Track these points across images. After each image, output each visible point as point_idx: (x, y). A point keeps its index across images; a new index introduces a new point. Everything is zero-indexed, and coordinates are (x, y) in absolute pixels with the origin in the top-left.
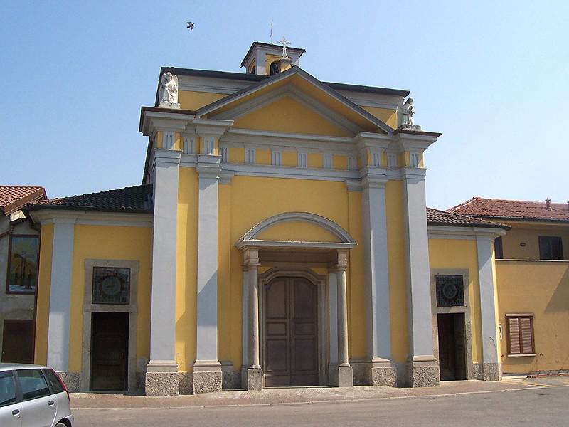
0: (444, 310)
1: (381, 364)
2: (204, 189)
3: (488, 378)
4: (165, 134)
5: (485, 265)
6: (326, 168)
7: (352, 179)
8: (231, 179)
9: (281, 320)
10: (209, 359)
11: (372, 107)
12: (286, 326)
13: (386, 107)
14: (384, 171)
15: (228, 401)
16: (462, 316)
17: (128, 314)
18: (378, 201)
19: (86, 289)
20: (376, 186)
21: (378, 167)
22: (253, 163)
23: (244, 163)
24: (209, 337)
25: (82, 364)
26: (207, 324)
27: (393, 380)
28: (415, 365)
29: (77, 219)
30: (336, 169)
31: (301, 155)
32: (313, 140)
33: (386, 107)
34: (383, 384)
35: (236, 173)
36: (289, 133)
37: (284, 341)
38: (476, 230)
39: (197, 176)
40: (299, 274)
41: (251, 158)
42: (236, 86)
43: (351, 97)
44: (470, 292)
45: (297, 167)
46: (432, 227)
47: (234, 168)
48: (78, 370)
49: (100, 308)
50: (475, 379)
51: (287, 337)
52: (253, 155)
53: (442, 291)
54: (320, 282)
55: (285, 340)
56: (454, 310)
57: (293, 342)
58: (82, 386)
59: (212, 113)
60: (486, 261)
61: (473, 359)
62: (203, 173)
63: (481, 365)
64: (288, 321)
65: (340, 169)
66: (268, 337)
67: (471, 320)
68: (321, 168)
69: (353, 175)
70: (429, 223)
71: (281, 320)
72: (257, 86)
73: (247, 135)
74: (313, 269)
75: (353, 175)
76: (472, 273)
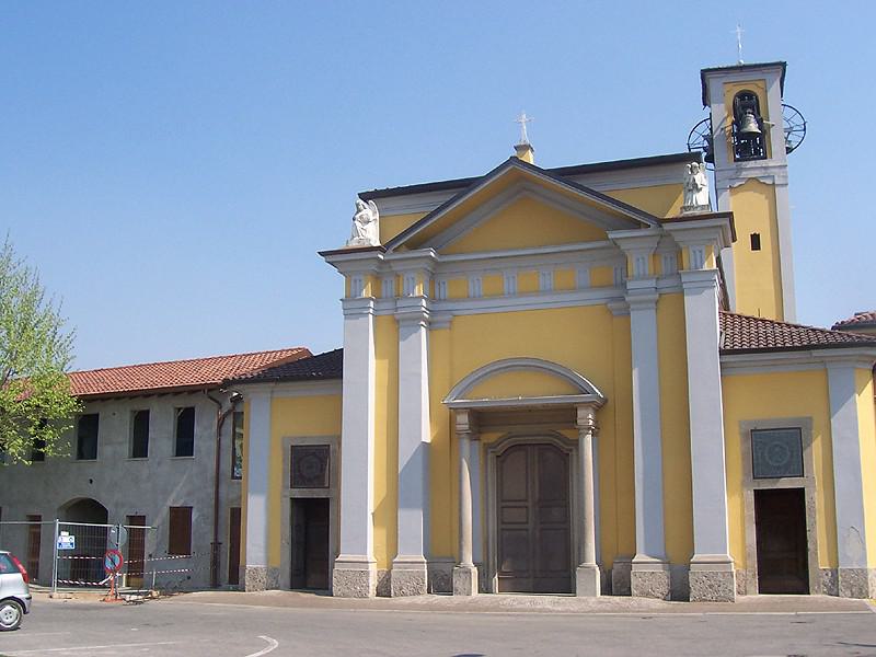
0: (766, 485)
1: (646, 566)
2: (406, 338)
3: (847, 593)
4: (353, 278)
5: (844, 407)
6: (514, 293)
7: (613, 299)
8: (451, 322)
9: (508, 504)
10: (413, 554)
11: (636, 194)
12: (527, 512)
13: (668, 182)
14: (653, 283)
15: (431, 608)
16: (800, 493)
17: (328, 499)
18: (644, 325)
19: (284, 472)
20: (643, 306)
21: (644, 277)
22: (644, 274)
23: (468, 298)
24: (413, 522)
25: (283, 559)
26: (409, 506)
27: (665, 589)
28: (635, 568)
29: (272, 392)
30: (592, 288)
31: (508, 278)
32: (579, 250)
33: (668, 182)
34: (647, 595)
35: (456, 313)
36: (524, 248)
37: (525, 532)
38: (814, 354)
39: (396, 326)
40: (547, 440)
41: (511, 287)
42: (439, 199)
43: (587, 181)
44: (815, 454)
45: (538, 293)
46: (728, 358)
47: (450, 306)
48: (276, 564)
49: (299, 493)
50: (824, 593)
51: (530, 526)
52: (644, 264)
53: (762, 454)
54: (571, 450)
55: (527, 530)
56: (785, 483)
57: (538, 534)
58: (281, 581)
59: (411, 241)
60: (847, 399)
61: (819, 560)
62: (404, 320)
63: (835, 572)
64: (530, 504)
65: (592, 287)
66: (504, 526)
67: (816, 502)
68: (574, 290)
69: (615, 293)
70: (722, 352)
71: (508, 504)
72: (466, 193)
73: (463, 261)
74: (562, 432)
75: (615, 293)
76: (818, 422)
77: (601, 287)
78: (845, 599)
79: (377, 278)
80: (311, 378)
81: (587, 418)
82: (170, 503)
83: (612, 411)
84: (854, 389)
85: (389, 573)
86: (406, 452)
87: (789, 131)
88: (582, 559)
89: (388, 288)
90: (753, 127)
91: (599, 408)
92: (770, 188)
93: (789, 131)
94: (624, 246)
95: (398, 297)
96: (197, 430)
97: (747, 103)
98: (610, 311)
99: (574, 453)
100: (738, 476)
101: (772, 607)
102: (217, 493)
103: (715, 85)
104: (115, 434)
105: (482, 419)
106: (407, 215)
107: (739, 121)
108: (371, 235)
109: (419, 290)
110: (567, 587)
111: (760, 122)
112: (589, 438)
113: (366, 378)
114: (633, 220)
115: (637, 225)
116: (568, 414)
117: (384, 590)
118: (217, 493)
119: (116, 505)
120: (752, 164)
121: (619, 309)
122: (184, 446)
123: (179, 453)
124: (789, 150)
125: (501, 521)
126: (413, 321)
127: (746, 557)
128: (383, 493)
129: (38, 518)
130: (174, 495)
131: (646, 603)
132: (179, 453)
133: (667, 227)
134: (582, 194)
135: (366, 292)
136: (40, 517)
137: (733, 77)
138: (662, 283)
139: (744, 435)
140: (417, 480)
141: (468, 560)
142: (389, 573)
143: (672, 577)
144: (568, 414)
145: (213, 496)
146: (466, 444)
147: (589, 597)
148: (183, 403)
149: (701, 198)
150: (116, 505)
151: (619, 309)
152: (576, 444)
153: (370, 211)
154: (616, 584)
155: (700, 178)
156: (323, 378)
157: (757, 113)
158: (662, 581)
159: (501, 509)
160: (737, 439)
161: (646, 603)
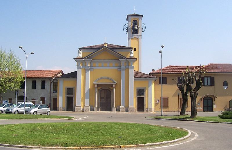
0: (139, 96)
10: (87, 105)
11: (122, 53)
14: (125, 67)
16: (144, 98)
18: (123, 73)
24: (87, 101)
25: (65, 106)
26: (87, 98)
34: (122, 111)
39: (85, 70)
42: (93, 51)
44: (146, 93)
49: (68, 96)
56: (142, 96)
59: (88, 57)
61: (146, 107)
63: (148, 109)
67: (146, 99)
76: (147, 88)
77: (117, 66)
78: (149, 112)
79: (82, 62)
80: (70, 78)
81: (114, 86)
82: (41, 97)
83: (118, 85)
84: (152, 84)
85: (84, 108)
86: (87, 90)
87: (143, 28)
88: (113, 106)
89: (84, 64)
90: (136, 28)
91: (116, 85)
92: (138, 39)
93: (143, 28)
94: (121, 61)
95: (85, 66)
96: (46, 84)
97: (135, 22)
98: (118, 70)
99: (112, 91)
100: (135, 95)
101: (140, 113)
102: (50, 96)
103: (129, 18)
104: (39, 85)
105: (98, 85)
106: (88, 53)
107: (134, 26)
108: (81, 56)
109: (89, 65)
110: (110, 110)
111: (137, 27)
112: (115, 89)
113: (80, 77)
114: (122, 57)
115: (123, 58)
116: (112, 85)
117: (83, 111)
118: (50, 96)
119: (29, 97)
120: (135, 34)
121: (120, 70)
122: (43, 87)
123: (42, 88)
124: (142, 32)
125: (100, 100)
126: (88, 70)
127: (136, 106)
128: (83, 96)
129: (35, 99)
130: (41, 95)
131: (122, 112)
132: (42, 88)
133: (128, 59)
134: (113, 52)
135: (81, 65)
136: (35, 99)
137: (133, 17)
138: (126, 67)
139: (136, 89)
140: (88, 95)
141: (96, 106)
142: (84, 108)
143: (126, 109)
144: (112, 85)
145: (50, 96)
146: (96, 89)
147: (114, 112)
148: (43, 80)
149: (133, 55)
150: (29, 97)
151: (120, 70)
152: (113, 90)
153: (81, 52)
154: (118, 110)
155: (133, 52)
156: (74, 78)
157: (137, 25)
158: (125, 110)
159: (100, 99)
160: (135, 90)
161: (122, 112)
